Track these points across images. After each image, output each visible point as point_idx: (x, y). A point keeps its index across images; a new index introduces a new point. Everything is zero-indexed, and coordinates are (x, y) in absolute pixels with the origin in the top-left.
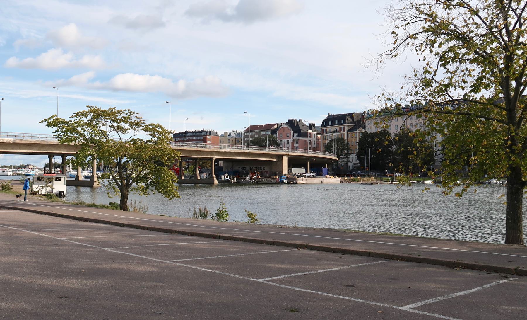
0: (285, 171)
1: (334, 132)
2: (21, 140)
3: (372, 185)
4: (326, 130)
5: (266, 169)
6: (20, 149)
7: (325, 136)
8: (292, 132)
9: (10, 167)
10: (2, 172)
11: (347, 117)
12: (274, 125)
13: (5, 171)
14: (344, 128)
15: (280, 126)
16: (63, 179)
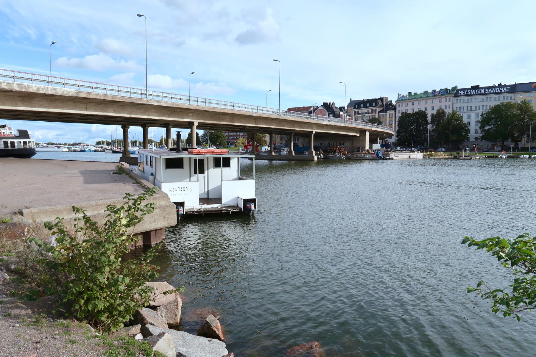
0: (367, 147)
1: (366, 113)
2: (89, 93)
3: (472, 160)
4: (358, 112)
5: (348, 144)
6: (86, 109)
7: (358, 117)
8: (327, 113)
9: (65, 144)
10: (57, 148)
11: (378, 100)
12: (311, 107)
13: (61, 147)
14: (376, 110)
15: (318, 108)
16: (234, 163)
